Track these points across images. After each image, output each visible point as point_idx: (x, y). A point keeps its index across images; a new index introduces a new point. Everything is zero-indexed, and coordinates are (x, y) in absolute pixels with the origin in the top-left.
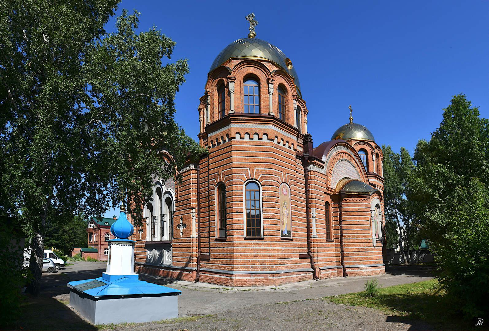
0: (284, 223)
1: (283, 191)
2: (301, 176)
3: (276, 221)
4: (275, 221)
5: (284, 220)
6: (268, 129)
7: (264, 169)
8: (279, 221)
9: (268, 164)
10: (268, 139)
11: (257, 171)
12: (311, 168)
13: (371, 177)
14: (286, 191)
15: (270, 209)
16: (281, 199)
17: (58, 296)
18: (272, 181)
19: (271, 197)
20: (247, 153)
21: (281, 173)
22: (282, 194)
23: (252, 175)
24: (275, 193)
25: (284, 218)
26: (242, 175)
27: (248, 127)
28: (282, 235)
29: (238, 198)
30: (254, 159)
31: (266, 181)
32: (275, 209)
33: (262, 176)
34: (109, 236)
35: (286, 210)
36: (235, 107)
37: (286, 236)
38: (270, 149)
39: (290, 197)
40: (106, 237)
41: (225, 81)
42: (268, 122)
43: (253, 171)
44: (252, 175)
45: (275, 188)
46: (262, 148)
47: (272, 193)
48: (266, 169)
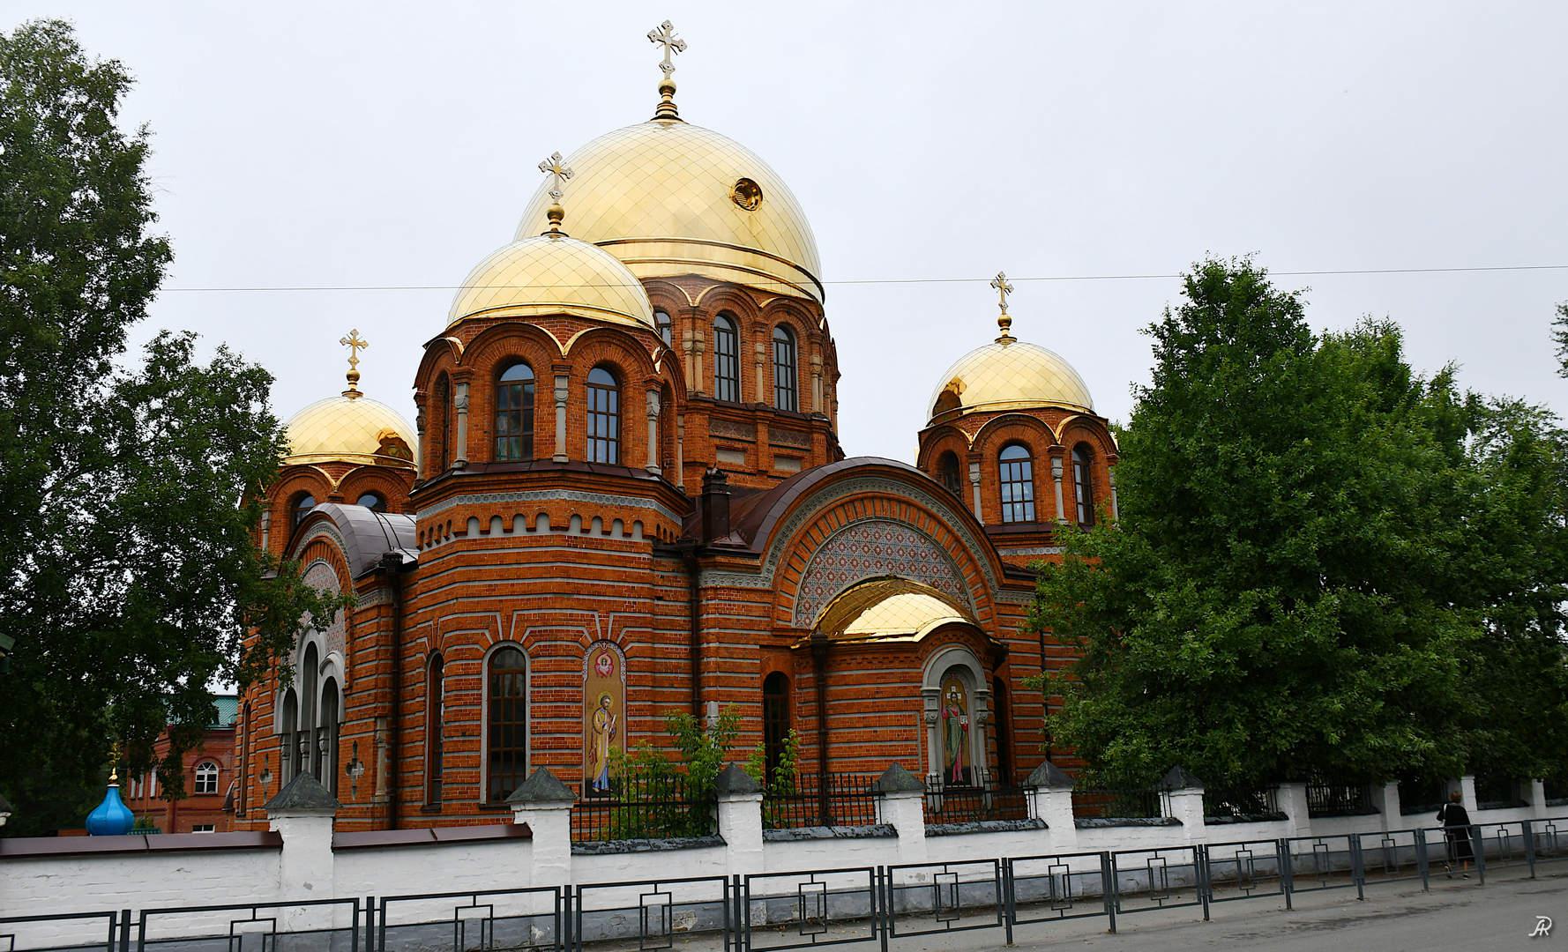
0: (599, 754)
1: (597, 664)
2: (674, 608)
3: (567, 754)
4: (563, 754)
5: (599, 749)
6: (551, 501)
7: (536, 612)
8: (577, 754)
9: (548, 596)
10: (552, 529)
11: (521, 619)
12: (710, 579)
13: (1002, 540)
14: (609, 662)
15: (549, 723)
16: (593, 689)
17: (866, 614)
18: (558, 643)
19: (554, 689)
20: (496, 571)
21: (593, 616)
22: (593, 672)
23: (507, 632)
24: (568, 676)
25: (599, 742)
26: (480, 631)
27: (499, 500)
28: (590, 793)
29: (468, 695)
30: (512, 585)
31: (542, 644)
32: (563, 722)
33: (531, 632)
34: (216, 772)
35: (606, 719)
36: (469, 450)
37: (602, 793)
38: (554, 554)
39: (623, 677)
40: (201, 777)
41: (327, 475)
42: (550, 483)
43: (509, 618)
44: (507, 632)
45: (567, 661)
46: (534, 555)
47: (555, 676)
48: (543, 611)
